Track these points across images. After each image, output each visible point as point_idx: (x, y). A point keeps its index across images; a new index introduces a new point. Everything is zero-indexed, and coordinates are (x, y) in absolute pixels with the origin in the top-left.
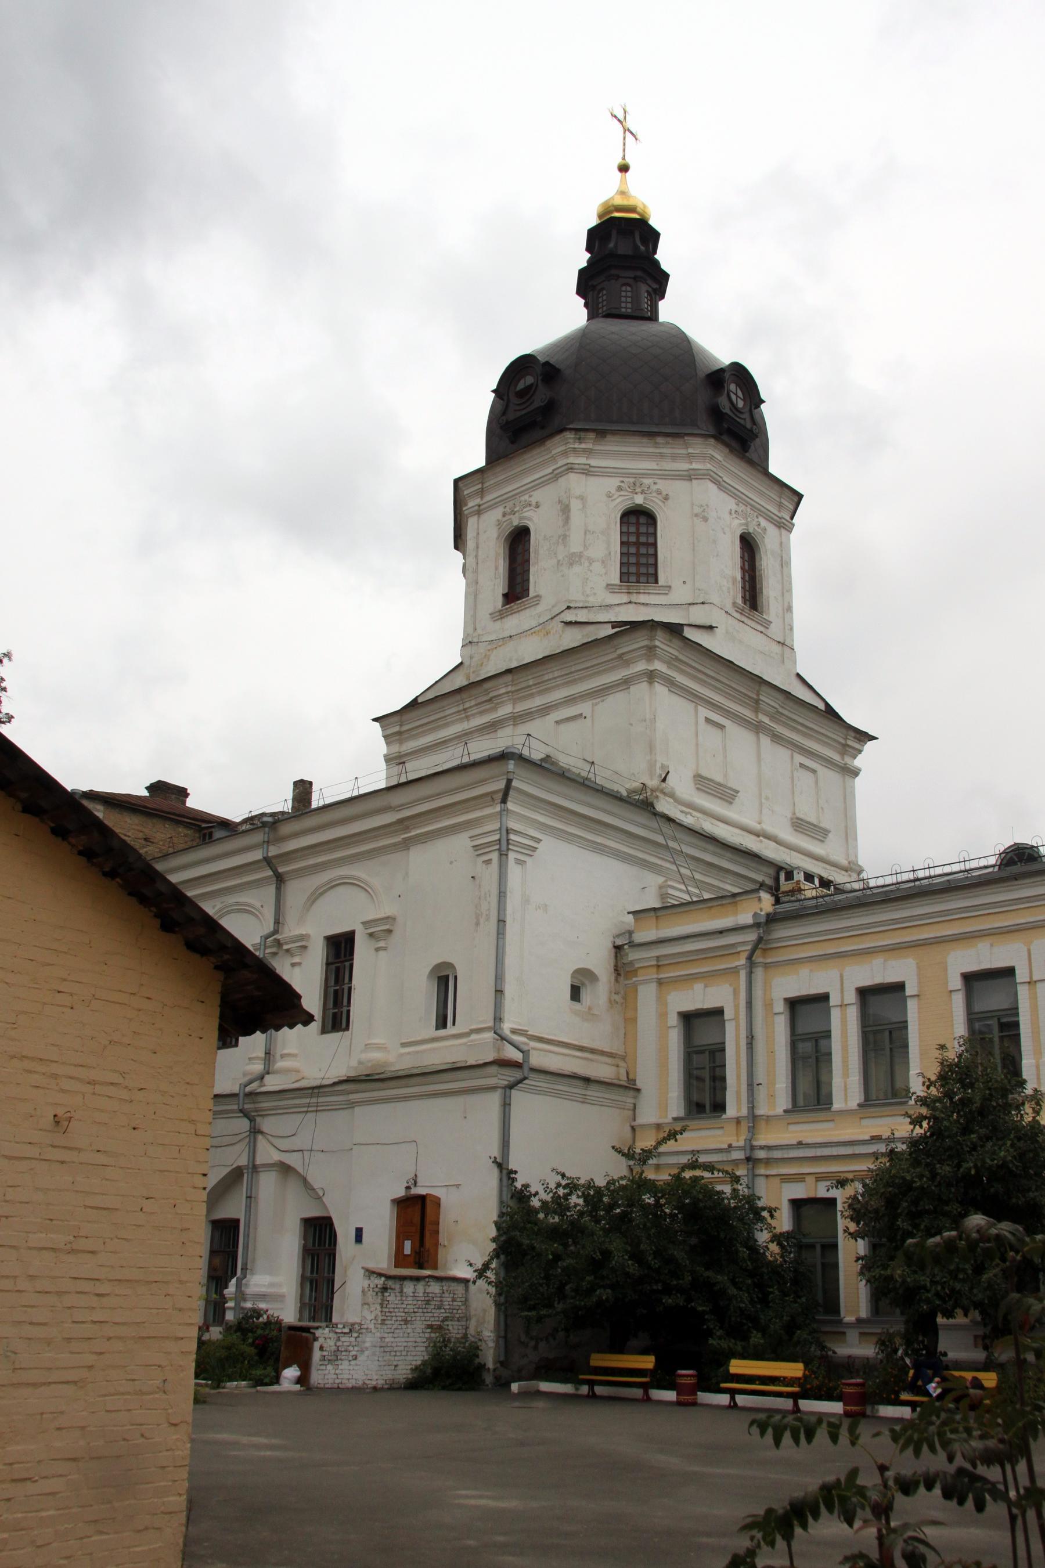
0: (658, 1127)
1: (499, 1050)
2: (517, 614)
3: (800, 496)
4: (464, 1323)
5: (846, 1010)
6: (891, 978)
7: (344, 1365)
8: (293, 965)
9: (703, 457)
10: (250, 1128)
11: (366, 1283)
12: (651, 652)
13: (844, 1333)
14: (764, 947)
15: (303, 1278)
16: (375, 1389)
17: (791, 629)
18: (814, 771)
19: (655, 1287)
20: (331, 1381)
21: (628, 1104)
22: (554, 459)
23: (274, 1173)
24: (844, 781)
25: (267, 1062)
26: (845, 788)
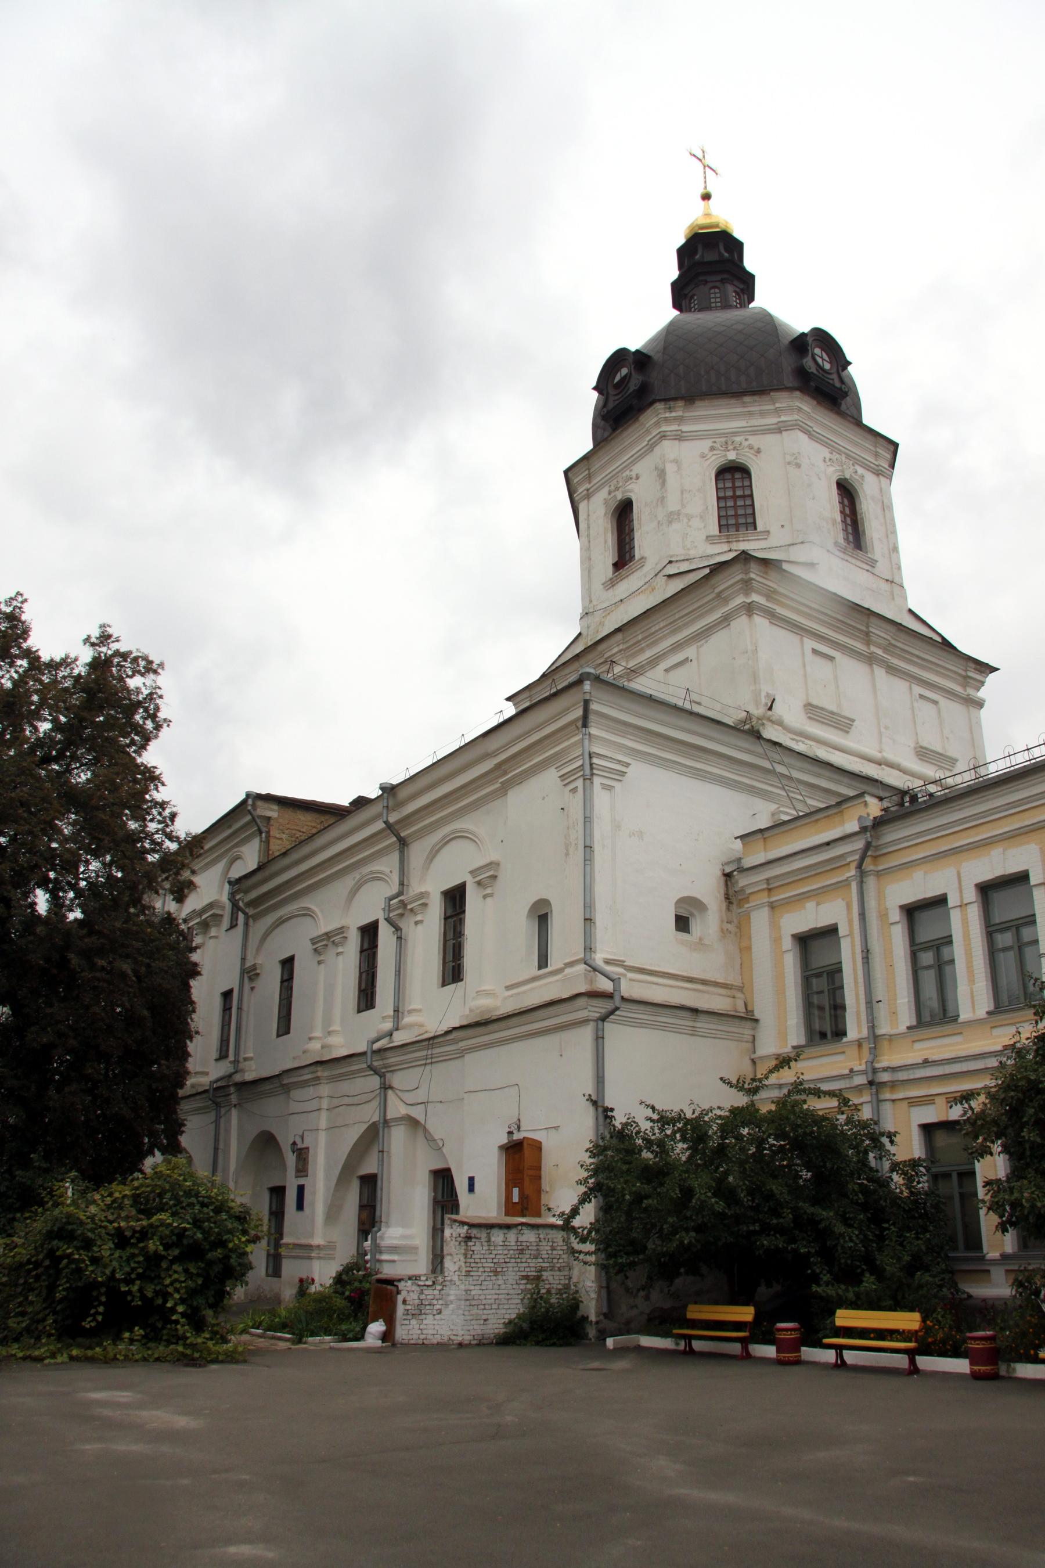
1: (591, 982)
2: (626, 580)
4: (566, 1273)
6: (1013, 867)
7: (429, 1320)
8: (417, 923)
9: (790, 409)
12: (747, 586)
13: (988, 1271)
14: (874, 854)
16: (461, 1345)
17: (899, 568)
18: (935, 702)
19: (752, 1228)
20: (415, 1337)
22: (648, 431)
23: (402, 1128)
24: (969, 712)
26: (970, 719)
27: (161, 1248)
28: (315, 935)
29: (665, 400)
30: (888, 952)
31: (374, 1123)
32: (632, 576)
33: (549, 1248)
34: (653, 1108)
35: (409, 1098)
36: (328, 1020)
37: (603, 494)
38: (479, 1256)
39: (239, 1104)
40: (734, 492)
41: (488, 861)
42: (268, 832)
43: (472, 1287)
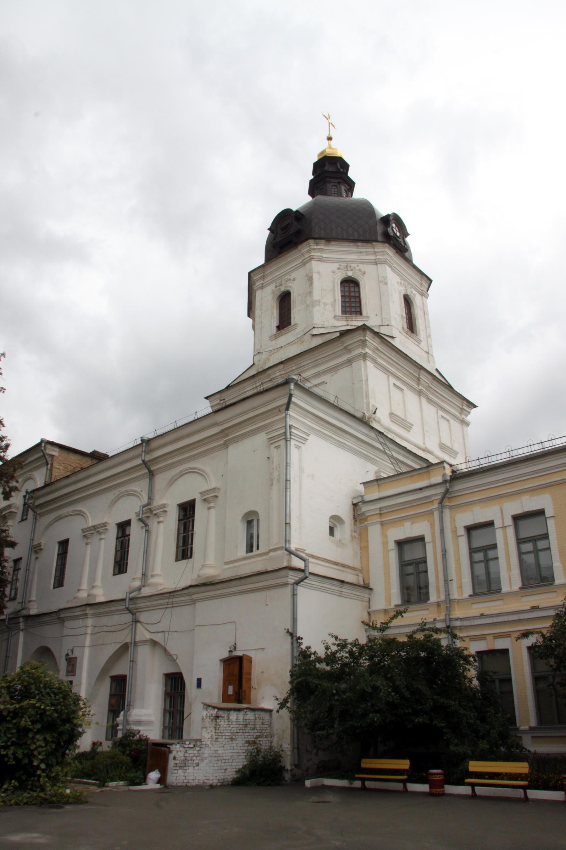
0: (386, 611)
4: (269, 739)
5: (506, 530)
7: (190, 770)
8: (159, 522)
10: (133, 619)
11: (204, 713)
15: (165, 710)
16: (212, 786)
19: (406, 711)
20: (181, 781)
21: (365, 598)
22: (303, 255)
24: (462, 427)
25: (143, 580)
27: (30, 723)
28: (85, 526)
29: (315, 239)
30: (457, 551)
32: (288, 334)
34: (336, 638)
35: (152, 628)
36: (92, 579)
37: (272, 287)
38: (223, 729)
39: (25, 629)
40: (350, 294)
42: (52, 464)
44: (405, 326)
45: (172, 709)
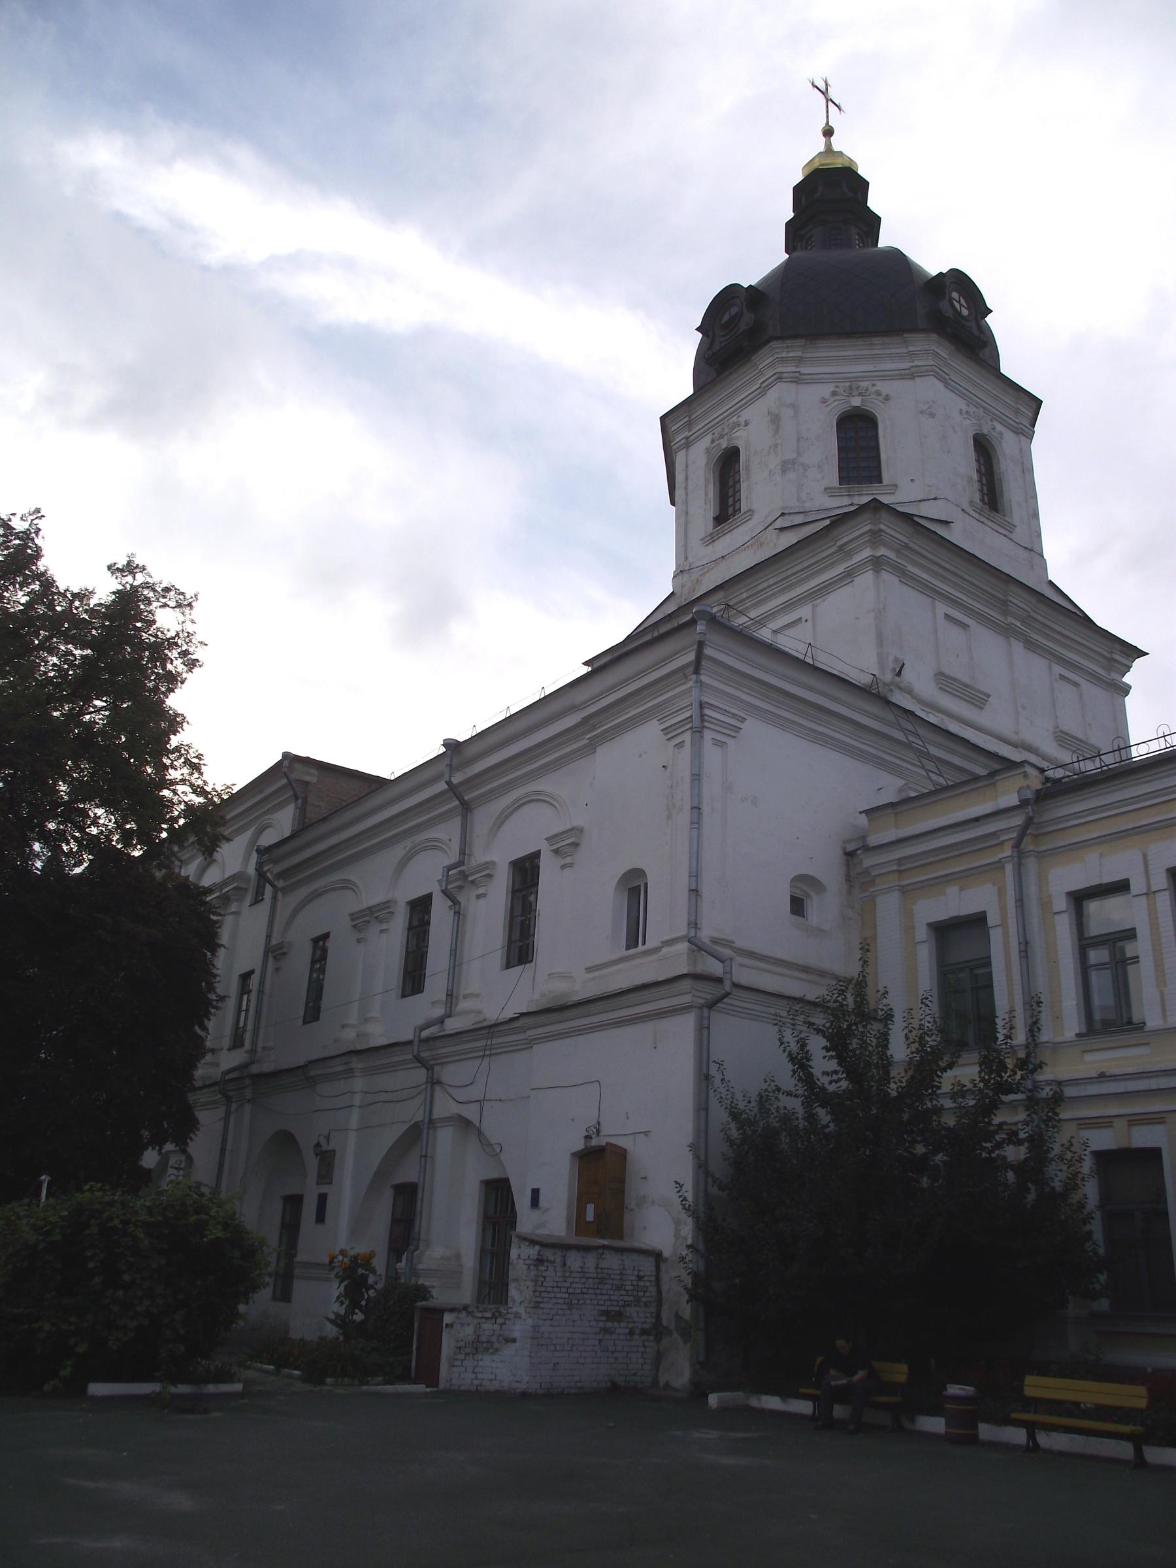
3: (1039, 403)
8: (479, 897)
10: (427, 1078)
14: (1035, 833)
16: (525, 1395)
18: (1076, 685)
22: (761, 373)
28: (356, 908)
31: (416, 1124)
33: (634, 1278)
35: (460, 1095)
37: (705, 442)
38: (551, 1284)
41: (568, 827)
43: (541, 1323)
44: (977, 497)
45: (496, 1248)
